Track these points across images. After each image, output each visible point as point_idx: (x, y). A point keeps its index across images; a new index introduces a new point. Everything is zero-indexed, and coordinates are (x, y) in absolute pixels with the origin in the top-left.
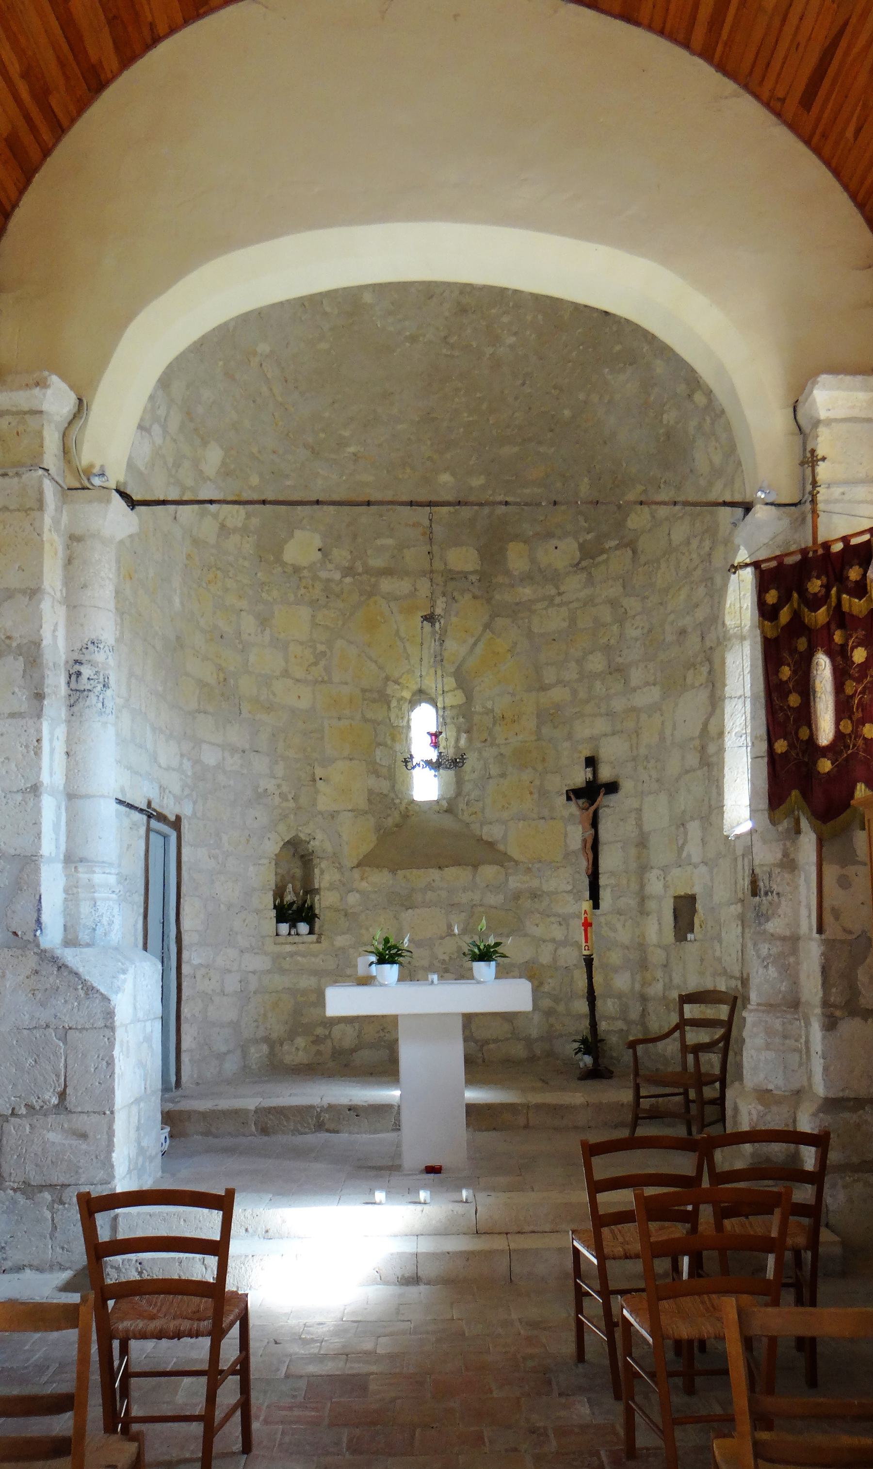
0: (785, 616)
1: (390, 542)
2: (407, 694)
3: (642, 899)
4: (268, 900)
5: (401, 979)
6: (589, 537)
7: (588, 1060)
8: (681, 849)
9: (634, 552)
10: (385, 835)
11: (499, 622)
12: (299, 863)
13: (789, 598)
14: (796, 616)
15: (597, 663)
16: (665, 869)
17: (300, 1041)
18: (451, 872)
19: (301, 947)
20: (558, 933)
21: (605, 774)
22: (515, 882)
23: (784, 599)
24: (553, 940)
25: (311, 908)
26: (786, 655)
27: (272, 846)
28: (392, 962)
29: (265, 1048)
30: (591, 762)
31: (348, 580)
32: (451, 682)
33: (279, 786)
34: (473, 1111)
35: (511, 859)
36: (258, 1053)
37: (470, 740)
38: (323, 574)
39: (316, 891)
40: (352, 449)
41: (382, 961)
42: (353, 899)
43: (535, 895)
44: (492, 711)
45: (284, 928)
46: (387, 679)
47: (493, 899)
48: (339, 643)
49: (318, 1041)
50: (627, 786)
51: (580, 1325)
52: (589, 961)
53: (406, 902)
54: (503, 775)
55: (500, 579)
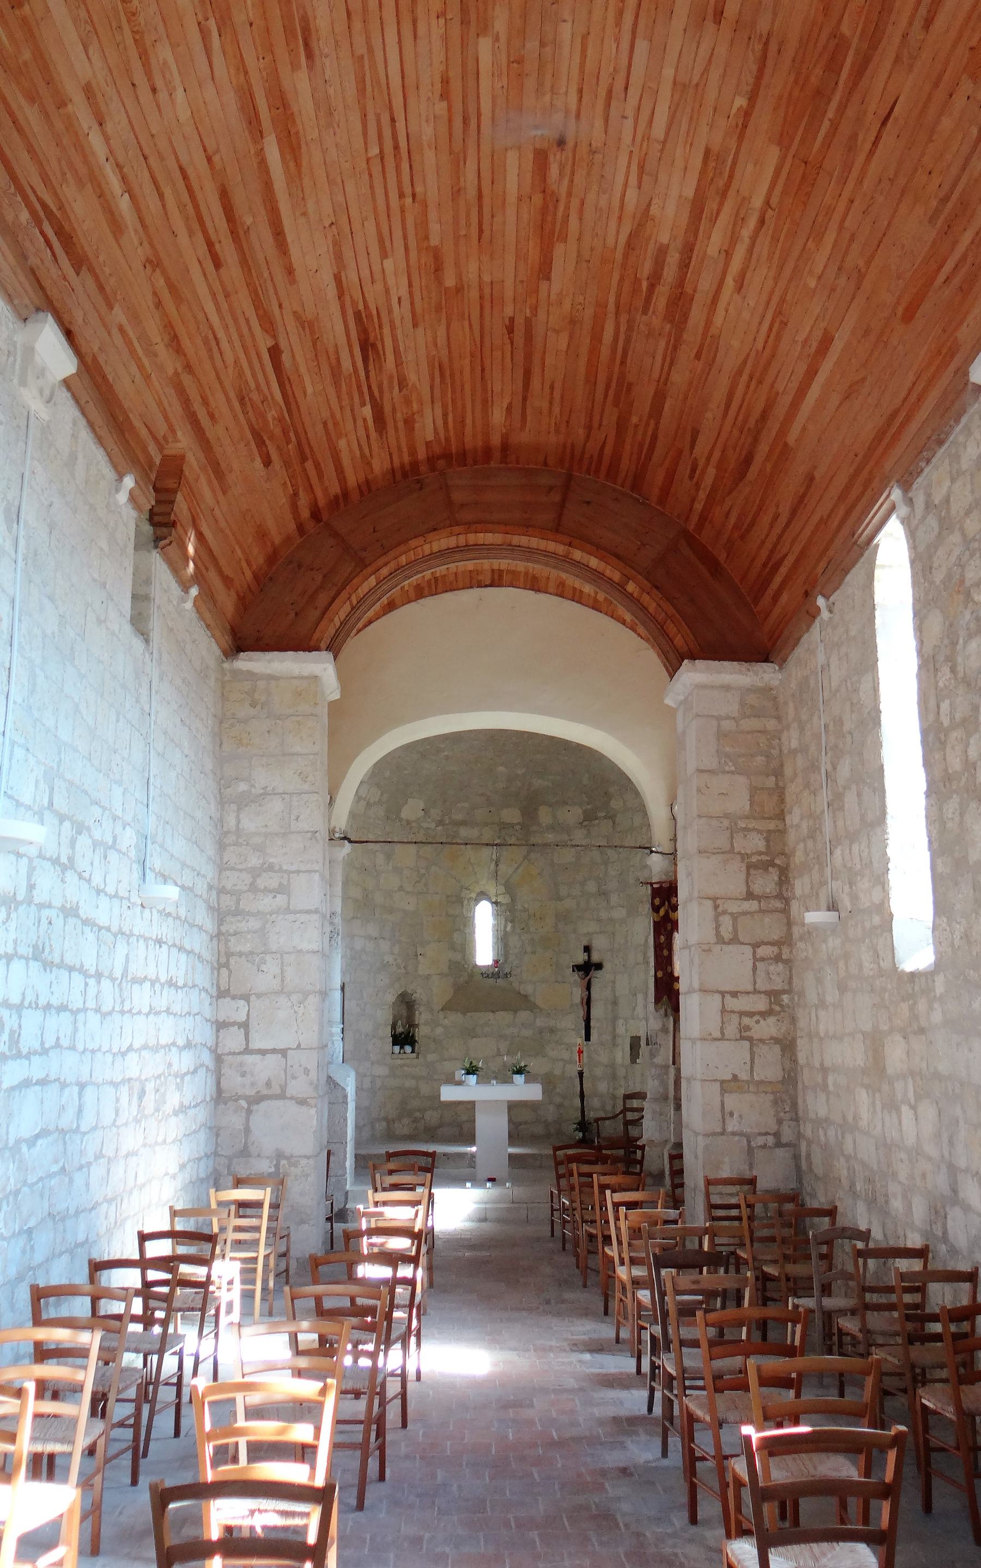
0: (662, 912)
1: (466, 805)
2: (473, 895)
3: (615, 1037)
4: (388, 1031)
5: (478, 1083)
6: (589, 807)
7: (581, 1135)
8: (634, 1009)
9: (614, 823)
10: (459, 989)
11: (533, 855)
12: (405, 1007)
13: (664, 904)
14: (667, 913)
15: (592, 887)
16: (626, 1020)
17: (406, 1121)
18: (501, 1014)
19: (408, 1061)
20: (566, 1056)
21: (595, 958)
22: (540, 1022)
23: (662, 904)
24: (562, 1060)
25: (413, 1036)
26: (662, 930)
27: (391, 998)
28: (473, 1073)
29: (384, 1124)
30: (587, 949)
31: (440, 828)
32: (502, 889)
33: (396, 960)
34: (511, 1156)
35: (538, 1007)
36: (381, 1126)
37: (513, 927)
38: (425, 825)
39: (417, 1026)
40: (446, 753)
41: (468, 1073)
42: (439, 1030)
43: (552, 1031)
44: (528, 910)
45: (397, 1048)
46: (462, 887)
47: (527, 1033)
48: (433, 868)
49: (415, 1120)
50: (607, 966)
51: (552, 1221)
52: (581, 1074)
53: (471, 1033)
54: (534, 953)
55: (534, 828)
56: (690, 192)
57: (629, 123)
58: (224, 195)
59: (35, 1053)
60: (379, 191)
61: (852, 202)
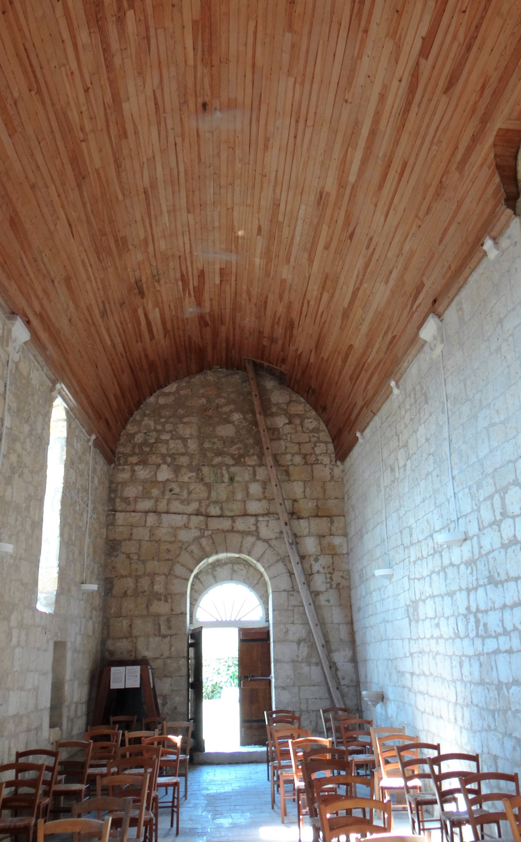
56: (125, 106)
57: (170, 127)
58: (380, 187)
59: (500, 634)
60: (314, 99)
61: (58, 196)
